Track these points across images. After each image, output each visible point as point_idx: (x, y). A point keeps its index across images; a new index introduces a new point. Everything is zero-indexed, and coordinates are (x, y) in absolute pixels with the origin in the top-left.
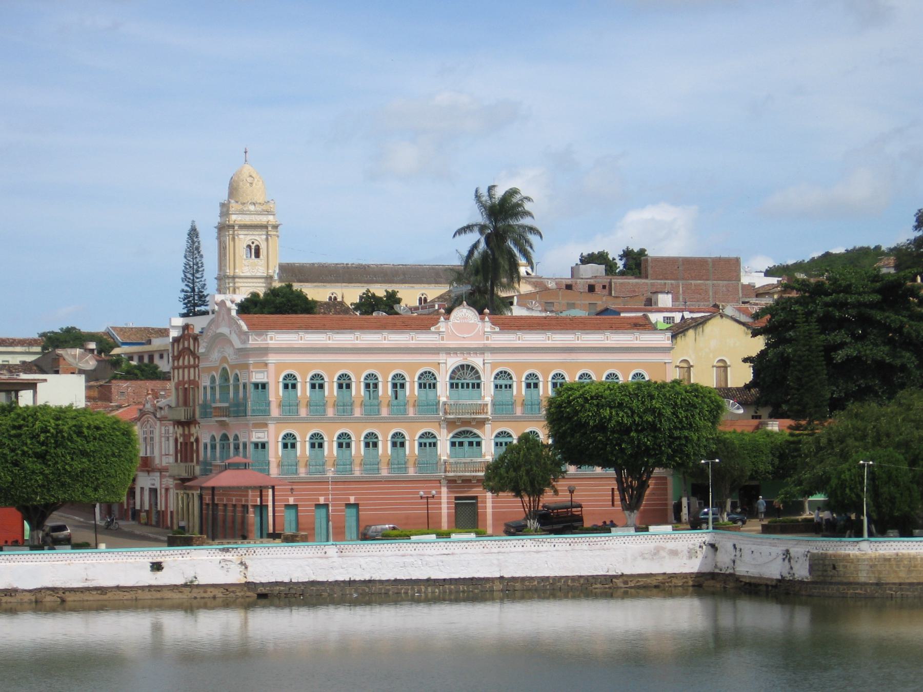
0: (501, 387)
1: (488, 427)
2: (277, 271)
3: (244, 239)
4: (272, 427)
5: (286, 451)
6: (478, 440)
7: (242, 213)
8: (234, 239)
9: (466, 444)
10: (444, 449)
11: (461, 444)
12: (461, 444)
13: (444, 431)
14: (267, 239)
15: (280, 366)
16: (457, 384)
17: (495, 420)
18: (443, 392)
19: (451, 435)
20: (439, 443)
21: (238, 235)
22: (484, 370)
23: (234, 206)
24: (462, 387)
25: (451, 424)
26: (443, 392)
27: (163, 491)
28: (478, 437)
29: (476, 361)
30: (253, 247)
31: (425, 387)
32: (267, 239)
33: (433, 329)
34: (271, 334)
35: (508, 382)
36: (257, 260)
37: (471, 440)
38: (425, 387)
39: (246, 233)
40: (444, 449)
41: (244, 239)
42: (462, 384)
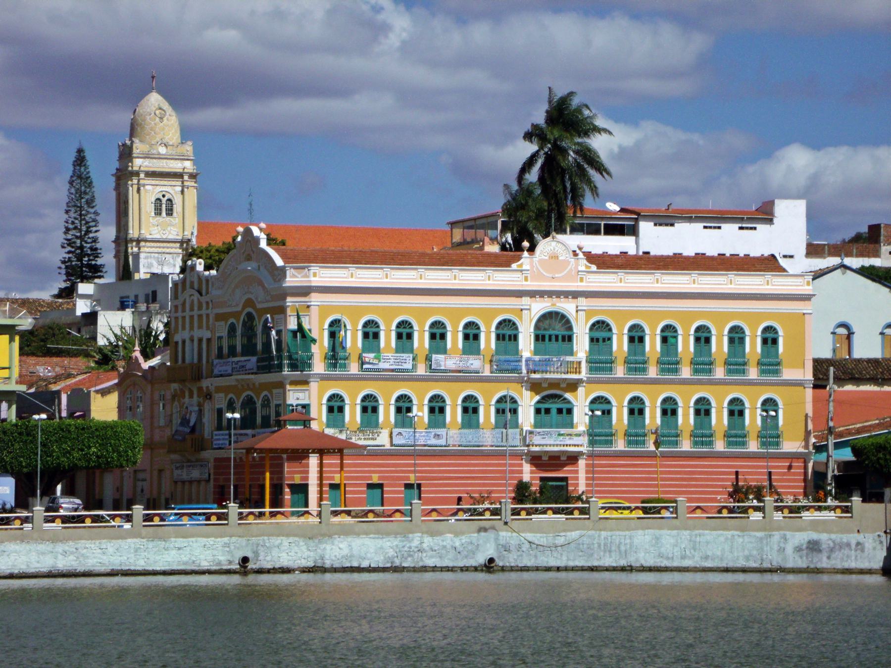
0: (598, 340)
1: (581, 390)
2: (195, 233)
3: (152, 190)
4: (314, 386)
5: (332, 416)
6: (568, 406)
7: (147, 156)
8: (139, 191)
9: (554, 412)
10: (526, 416)
11: (548, 411)
12: (548, 411)
13: (527, 394)
14: (182, 192)
15: (325, 310)
16: (543, 337)
17: (590, 381)
18: (526, 344)
19: (537, 398)
20: (520, 410)
21: (144, 185)
22: (577, 319)
23: (139, 147)
24: (550, 340)
25: (535, 387)
26: (526, 344)
27: (155, 473)
28: (569, 402)
29: (568, 307)
30: (164, 200)
31: (504, 339)
32: (182, 192)
33: (514, 266)
34: (315, 268)
35: (605, 334)
36: (169, 218)
37: (560, 406)
38: (504, 339)
39: (154, 182)
40: (526, 416)
41: (152, 190)
42: (550, 336)
